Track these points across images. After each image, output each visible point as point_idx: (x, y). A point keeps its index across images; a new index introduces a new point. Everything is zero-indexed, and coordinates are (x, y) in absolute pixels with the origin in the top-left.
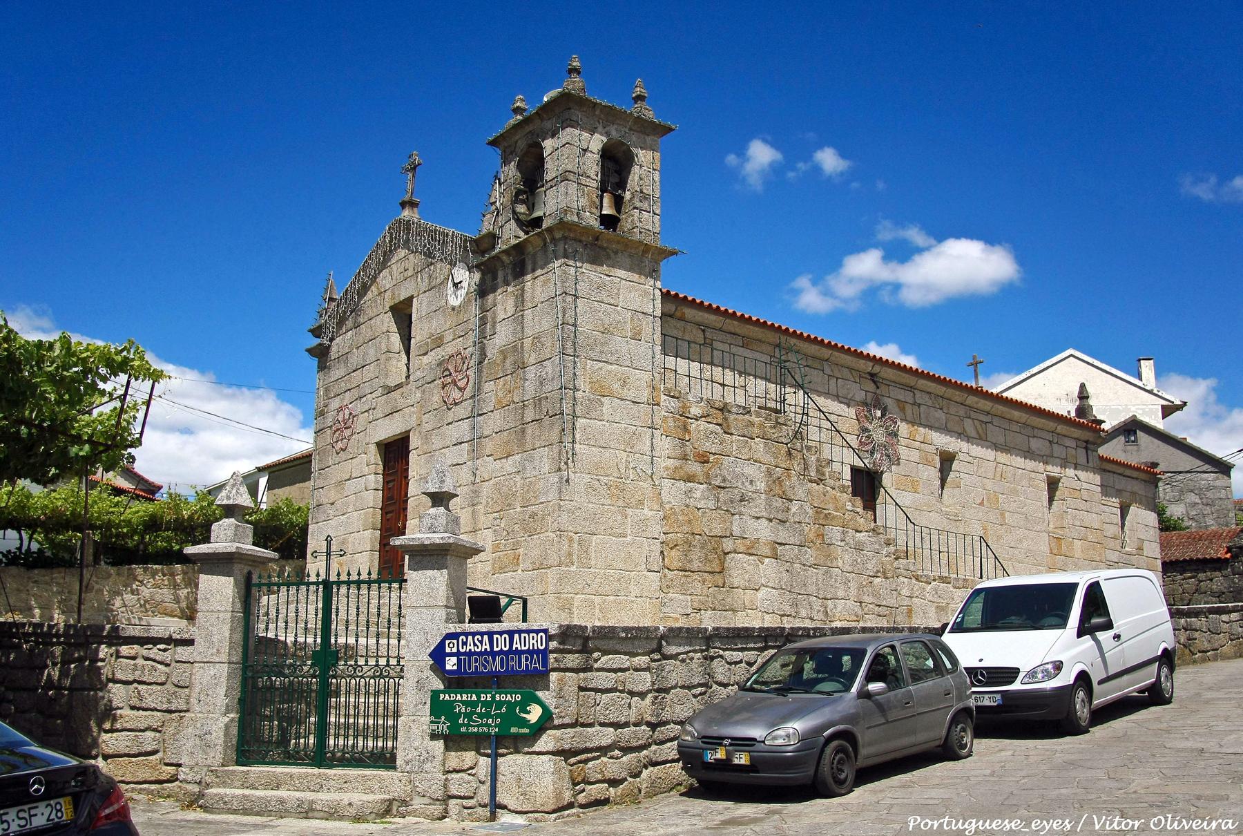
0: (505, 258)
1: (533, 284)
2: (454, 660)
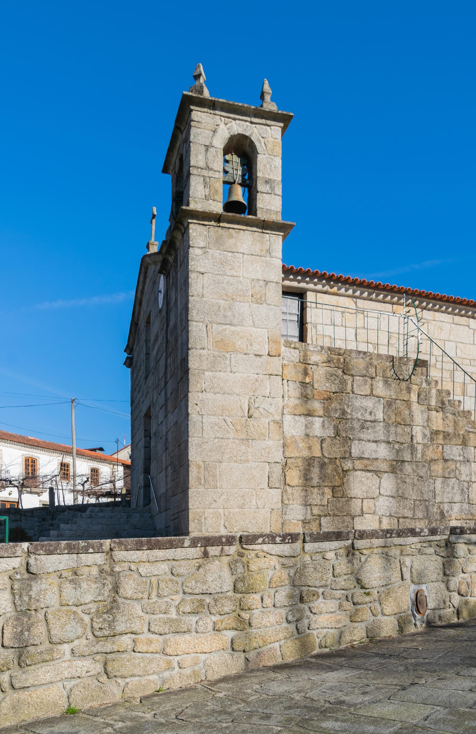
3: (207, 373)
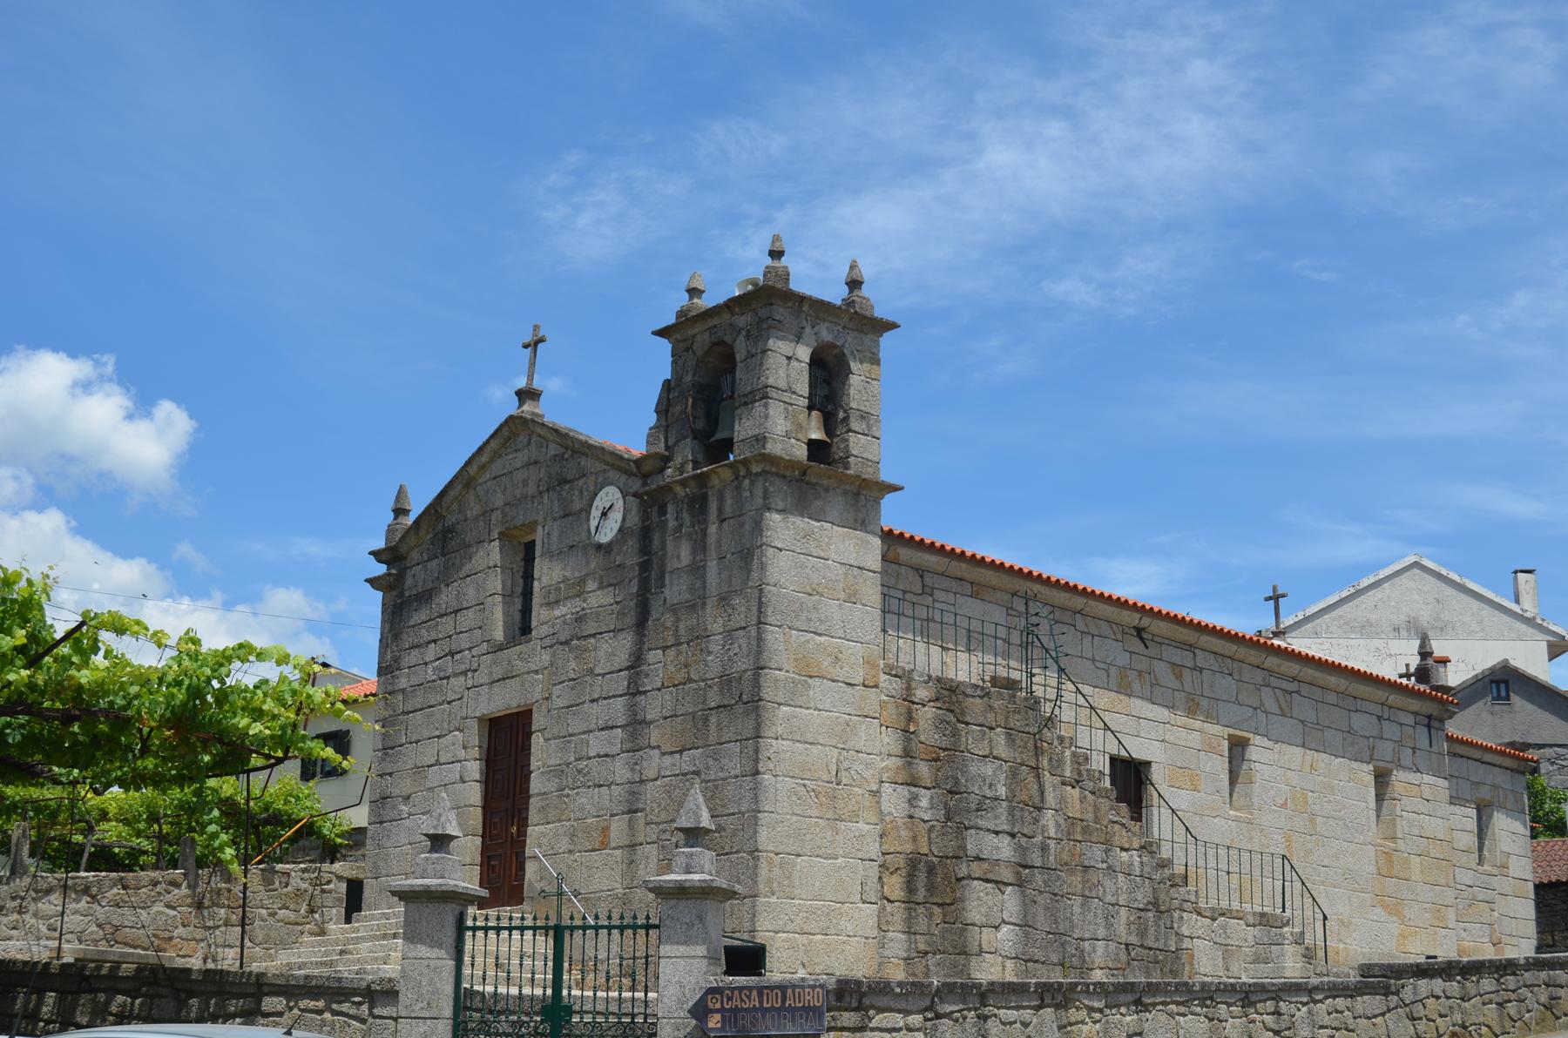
0: (679, 489)
1: (719, 529)
2: (718, 1017)
3: (784, 708)
